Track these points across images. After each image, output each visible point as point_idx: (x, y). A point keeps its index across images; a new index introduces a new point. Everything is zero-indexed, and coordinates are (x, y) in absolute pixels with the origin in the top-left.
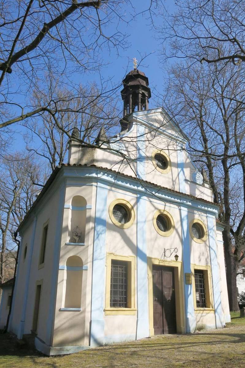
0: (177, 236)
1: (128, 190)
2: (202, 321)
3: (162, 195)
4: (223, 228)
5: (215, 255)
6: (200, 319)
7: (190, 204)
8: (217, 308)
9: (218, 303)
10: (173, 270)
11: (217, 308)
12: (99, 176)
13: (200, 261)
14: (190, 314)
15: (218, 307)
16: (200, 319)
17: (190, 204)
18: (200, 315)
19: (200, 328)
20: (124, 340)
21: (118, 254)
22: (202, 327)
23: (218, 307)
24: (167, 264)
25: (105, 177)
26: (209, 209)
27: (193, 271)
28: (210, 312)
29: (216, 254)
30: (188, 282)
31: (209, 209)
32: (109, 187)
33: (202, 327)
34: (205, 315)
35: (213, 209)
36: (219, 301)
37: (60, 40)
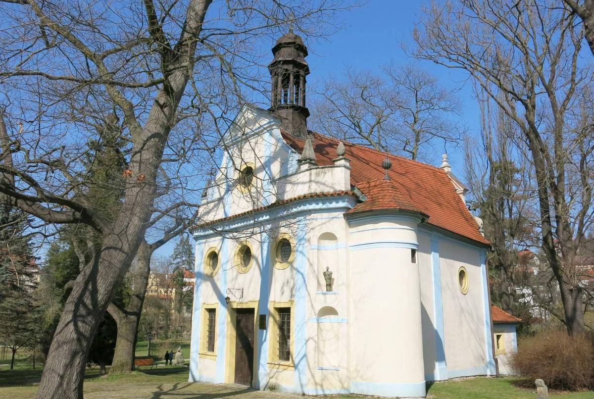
0: (257, 267)
1: (212, 236)
2: (277, 378)
3: (337, 202)
4: (420, 219)
5: (303, 279)
6: (274, 376)
7: (268, 217)
8: (298, 364)
9: (301, 356)
10: (251, 311)
11: (298, 364)
12: (259, 220)
13: (283, 293)
14: (263, 366)
15: (300, 361)
16: (274, 376)
17: (268, 217)
18: (275, 370)
19: (273, 388)
20: (208, 381)
21: (210, 303)
22: (275, 386)
23: (300, 361)
24: (244, 307)
25: (313, 206)
26: (295, 210)
27: (272, 310)
28: (287, 368)
29: (306, 279)
30: (263, 325)
31: (295, 210)
32: (204, 240)
33: (275, 386)
34: (282, 371)
35: (300, 206)
36: (303, 353)
37: (322, 9)
